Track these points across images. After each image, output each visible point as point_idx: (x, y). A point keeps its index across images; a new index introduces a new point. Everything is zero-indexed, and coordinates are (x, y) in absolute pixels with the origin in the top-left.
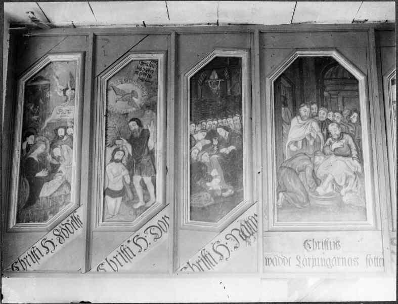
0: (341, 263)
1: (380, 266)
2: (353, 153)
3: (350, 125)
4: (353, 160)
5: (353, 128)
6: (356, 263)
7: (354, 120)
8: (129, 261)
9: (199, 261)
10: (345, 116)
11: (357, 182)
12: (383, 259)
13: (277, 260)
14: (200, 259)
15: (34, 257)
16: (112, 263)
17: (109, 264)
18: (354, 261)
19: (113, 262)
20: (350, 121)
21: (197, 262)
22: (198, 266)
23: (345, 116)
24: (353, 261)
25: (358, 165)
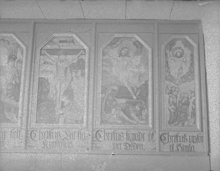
6: (185, 139)
9: (173, 136)
22: (172, 138)
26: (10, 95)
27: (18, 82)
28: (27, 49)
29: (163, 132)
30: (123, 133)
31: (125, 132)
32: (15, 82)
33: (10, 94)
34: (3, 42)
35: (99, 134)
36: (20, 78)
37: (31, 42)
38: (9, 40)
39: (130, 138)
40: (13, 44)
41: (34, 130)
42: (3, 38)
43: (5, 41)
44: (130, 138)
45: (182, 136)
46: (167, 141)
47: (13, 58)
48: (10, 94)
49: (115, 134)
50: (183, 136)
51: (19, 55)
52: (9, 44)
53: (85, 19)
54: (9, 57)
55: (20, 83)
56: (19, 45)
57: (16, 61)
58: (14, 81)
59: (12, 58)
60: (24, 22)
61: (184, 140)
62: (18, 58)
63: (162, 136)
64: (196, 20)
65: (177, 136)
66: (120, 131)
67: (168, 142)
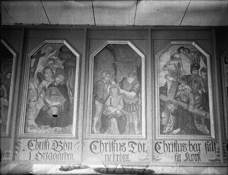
0: (108, 149)
1: (210, 151)
2: (5, 95)
3: (6, 80)
4: (4, 99)
5: (7, 81)
6: (185, 148)
7: (9, 77)
8: (44, 149)
9: (171, 144)
10: (4, 75)
11: (5, 111)
12: (140, 143)
13: (61, 156)
14: (172, 143)
15: (112, 148)
16: (102, 145)
17: (164, 145)
18: (183, 146)
19: (117, 145)
20: (6, 78)
21: (105, 143)
22: (39, 145)
23: (4, 75)
24: (182, 147)
25: (7, 101)
26: (198, 105)
27: (205, 92)
28: (211, 58)
29: (157, 141)
30: (185, 144)
31: (187, 142)
32: (202, 92)
33: (198, 104)
34: (183, 51)
35: (158, 145)
36: (206, 88)
37: (21, 48)
38: (189, 48)
39: (167, 147)
40: (195, 53)
41: (158, 143)
42: (182, 46)
43: (185, 50)
44: (167, 147)
45: (120, 144)
46: (98, 150)
47: (196, 66)
48: (198, 104)
49: (176, 145)
50: (121, 144)
51: (202, 65)
52: (189, 52)
53: (51, 25)
54: (191, 66)
55: (207, 93)
56: (200, 53)
57: (200, 70)
58: (200, 91)
59: (195, 66)
60: (78, 29)
61: (184, 149)
62: (201, 67)
63: (93, 144)
64: (72, 25)
65: (175, 144)
66: (182, 142)
67: (164, 151)
